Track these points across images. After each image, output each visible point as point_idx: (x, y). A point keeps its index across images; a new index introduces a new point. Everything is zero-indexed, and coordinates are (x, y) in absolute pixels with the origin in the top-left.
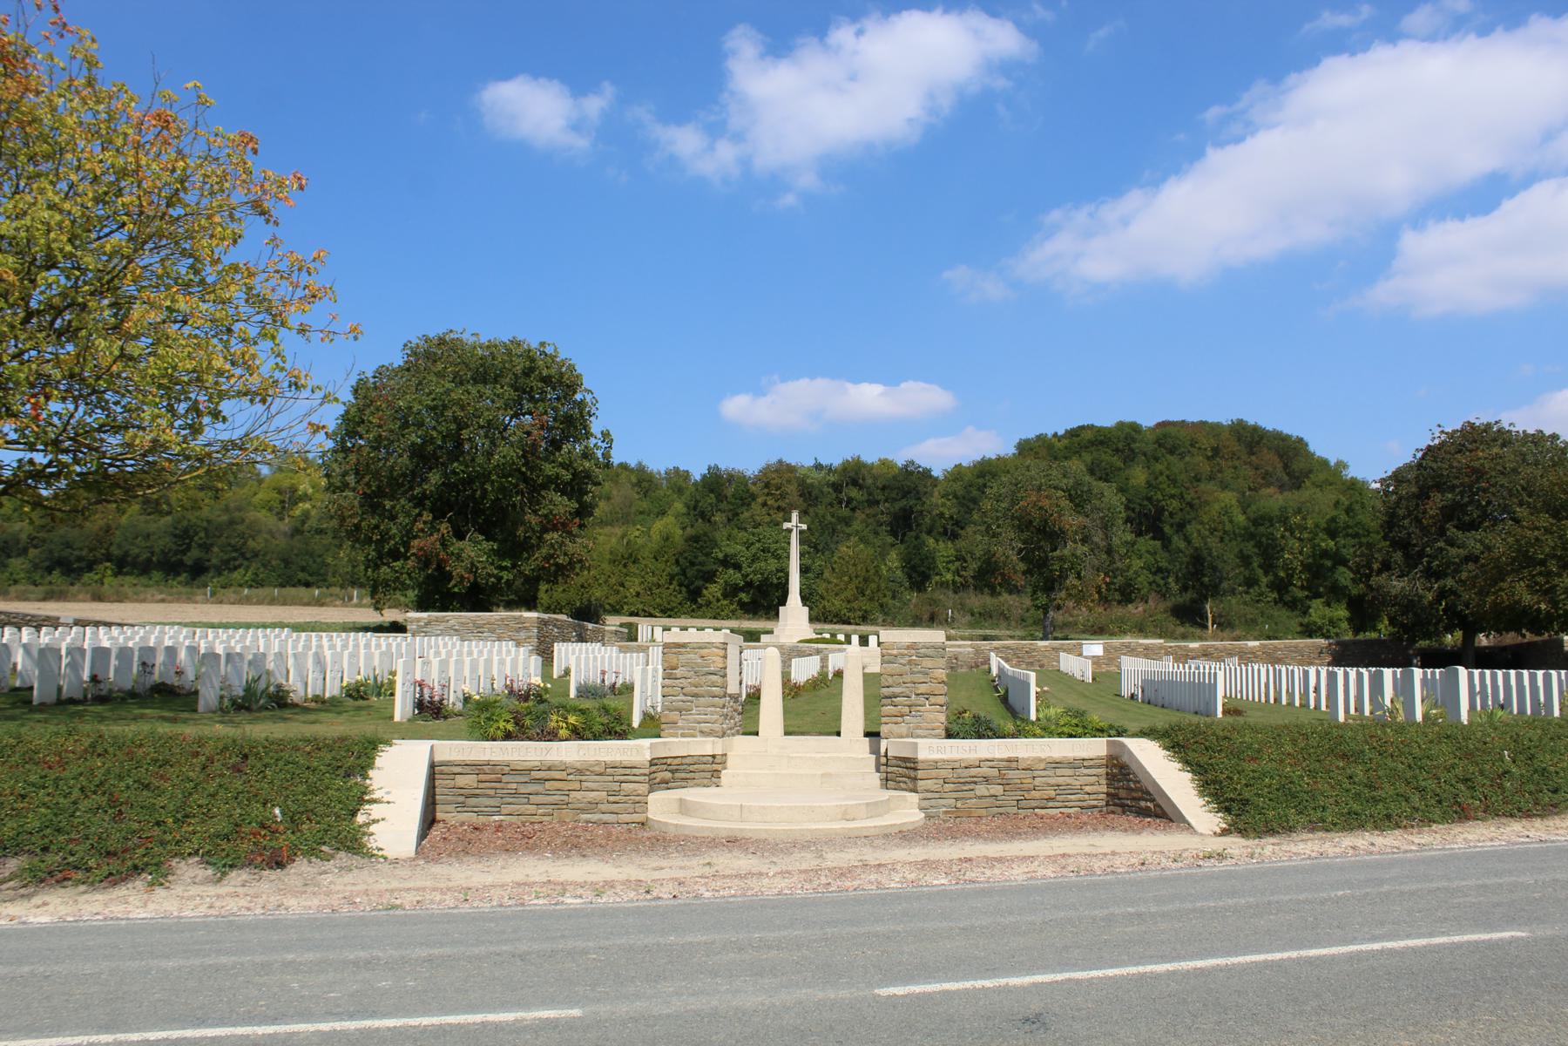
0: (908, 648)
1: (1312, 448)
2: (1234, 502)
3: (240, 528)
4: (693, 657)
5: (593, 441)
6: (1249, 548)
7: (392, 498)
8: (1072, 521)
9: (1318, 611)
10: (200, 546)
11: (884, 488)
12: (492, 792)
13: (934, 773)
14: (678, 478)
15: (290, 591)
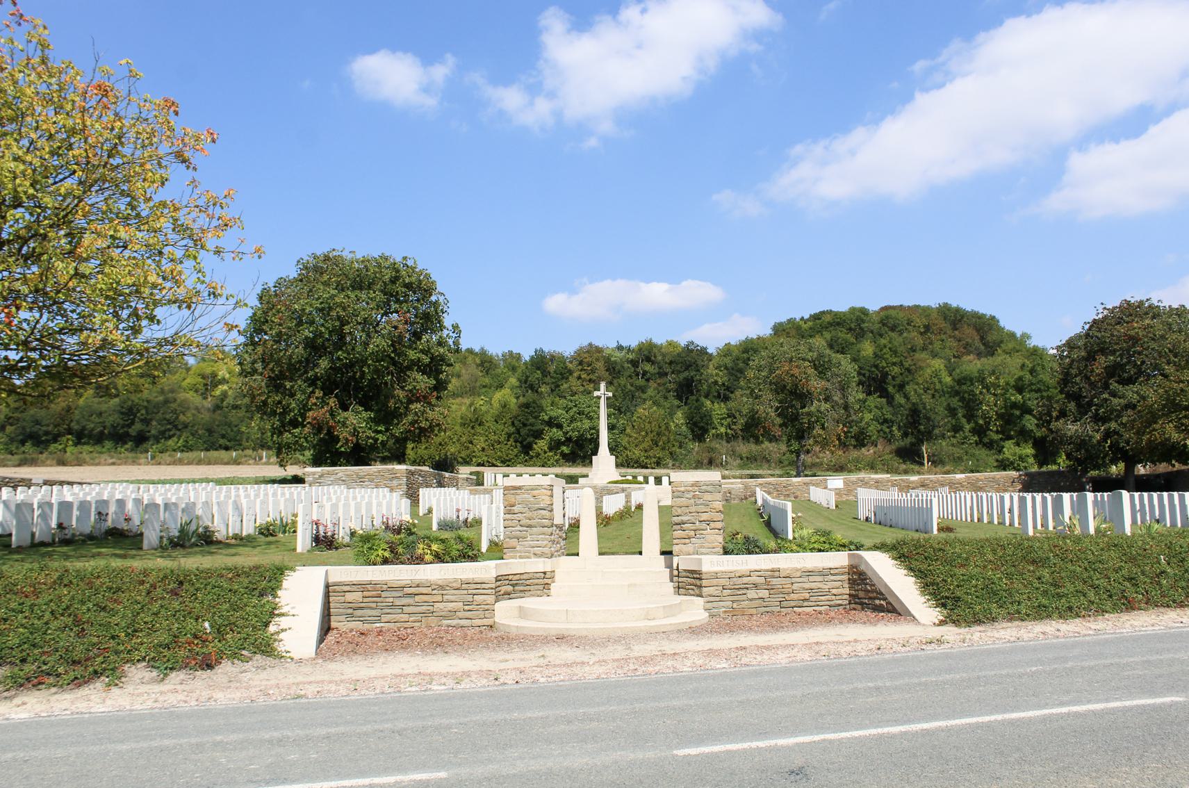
1: (1002, 324)
2: (942, 367)
3: (173, 406)
5: (445, 332)
6: (955, 402)
7: (291, 380)
10: (142, 420)
11: (671, 363)
12: (374, 605)
13: (715, 582)
14: (512, 360)
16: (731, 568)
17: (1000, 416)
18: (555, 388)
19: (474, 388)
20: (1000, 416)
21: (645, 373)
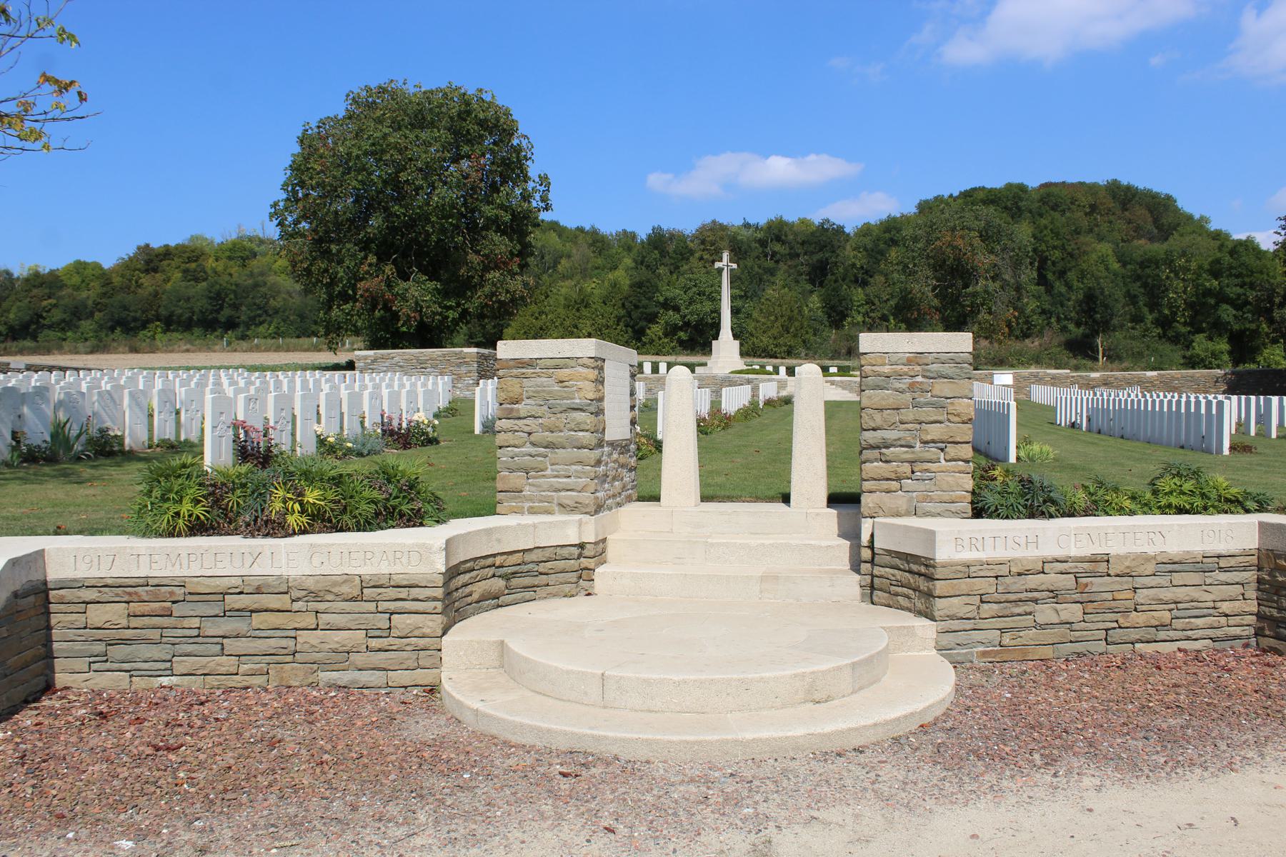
0: (909, 362)
1: (1179, 204)
2: (1110, 252)
3: (263, 289)
4: (546, 382)
5: (530, 185)
6: (1136, 288)
7: (339, 241)
8: (984, 260)
9: (1201, 344)
11: (803, 243)
12: (155, 635)
13: (964, 585)
14: (627, 239)
15: (305, 341)
16: (1000, 553)
17: (1190, 305)
18: (675, 269)
19: (585, 269)
20: (1190, 305)
21: (774, 254)
